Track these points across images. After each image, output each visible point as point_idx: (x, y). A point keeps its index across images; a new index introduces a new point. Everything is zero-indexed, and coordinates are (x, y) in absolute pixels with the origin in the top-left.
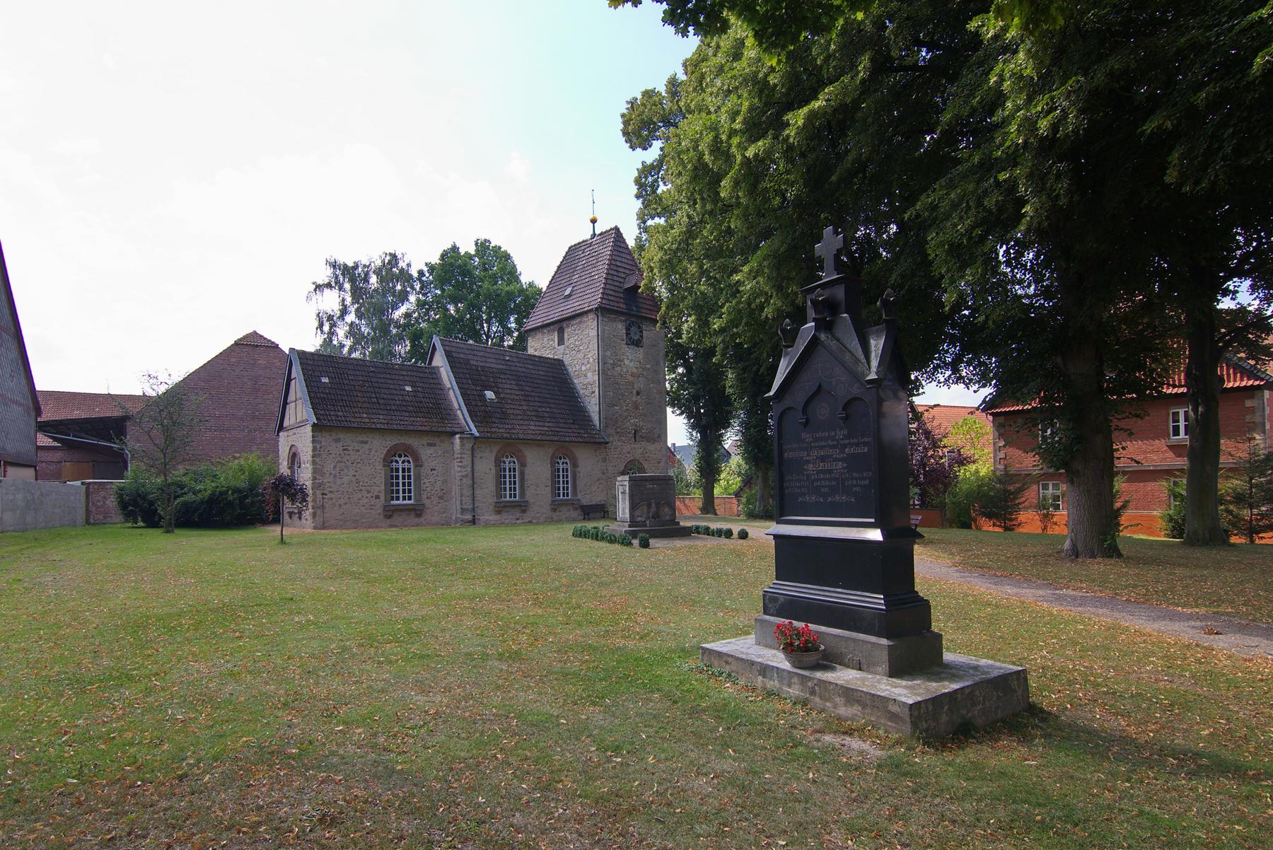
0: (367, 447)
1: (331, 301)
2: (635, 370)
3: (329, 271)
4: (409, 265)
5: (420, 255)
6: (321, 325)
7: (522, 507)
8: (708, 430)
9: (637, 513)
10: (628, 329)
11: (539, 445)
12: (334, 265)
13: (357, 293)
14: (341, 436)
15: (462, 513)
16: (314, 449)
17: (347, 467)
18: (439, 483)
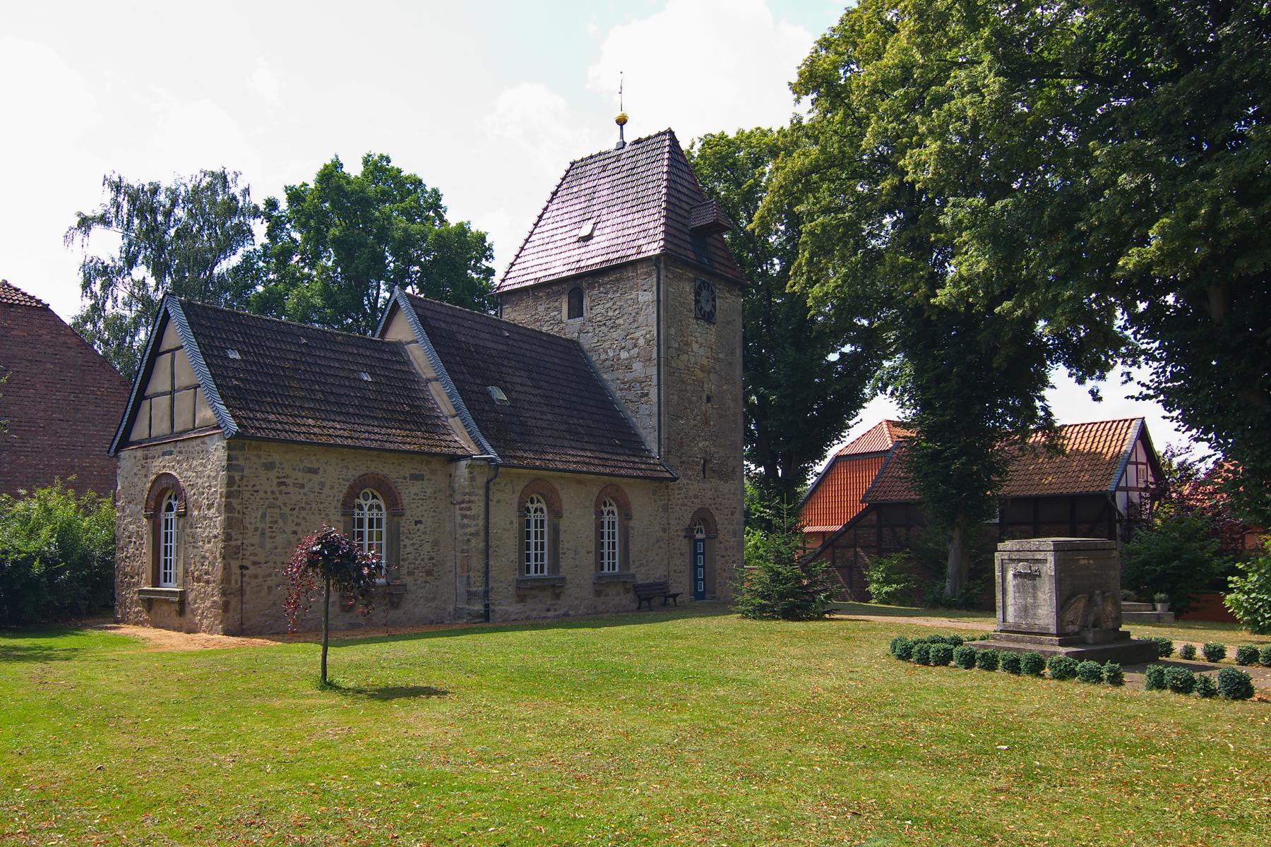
0: (317, 478)
1: (107, 244)
2: (705, 361)
3: (109, 195)
4: (246, 192)
5: (271, 171)
6: (86, 285)
7: (554, 587)
9: (1069, 616)
10: (697, 294)
11: (579, 482)
12: (117, 187)
13: (152, 234)
14: (276, 458)
15: (469, 601)
16: (230, 482)
18: (427, 547)
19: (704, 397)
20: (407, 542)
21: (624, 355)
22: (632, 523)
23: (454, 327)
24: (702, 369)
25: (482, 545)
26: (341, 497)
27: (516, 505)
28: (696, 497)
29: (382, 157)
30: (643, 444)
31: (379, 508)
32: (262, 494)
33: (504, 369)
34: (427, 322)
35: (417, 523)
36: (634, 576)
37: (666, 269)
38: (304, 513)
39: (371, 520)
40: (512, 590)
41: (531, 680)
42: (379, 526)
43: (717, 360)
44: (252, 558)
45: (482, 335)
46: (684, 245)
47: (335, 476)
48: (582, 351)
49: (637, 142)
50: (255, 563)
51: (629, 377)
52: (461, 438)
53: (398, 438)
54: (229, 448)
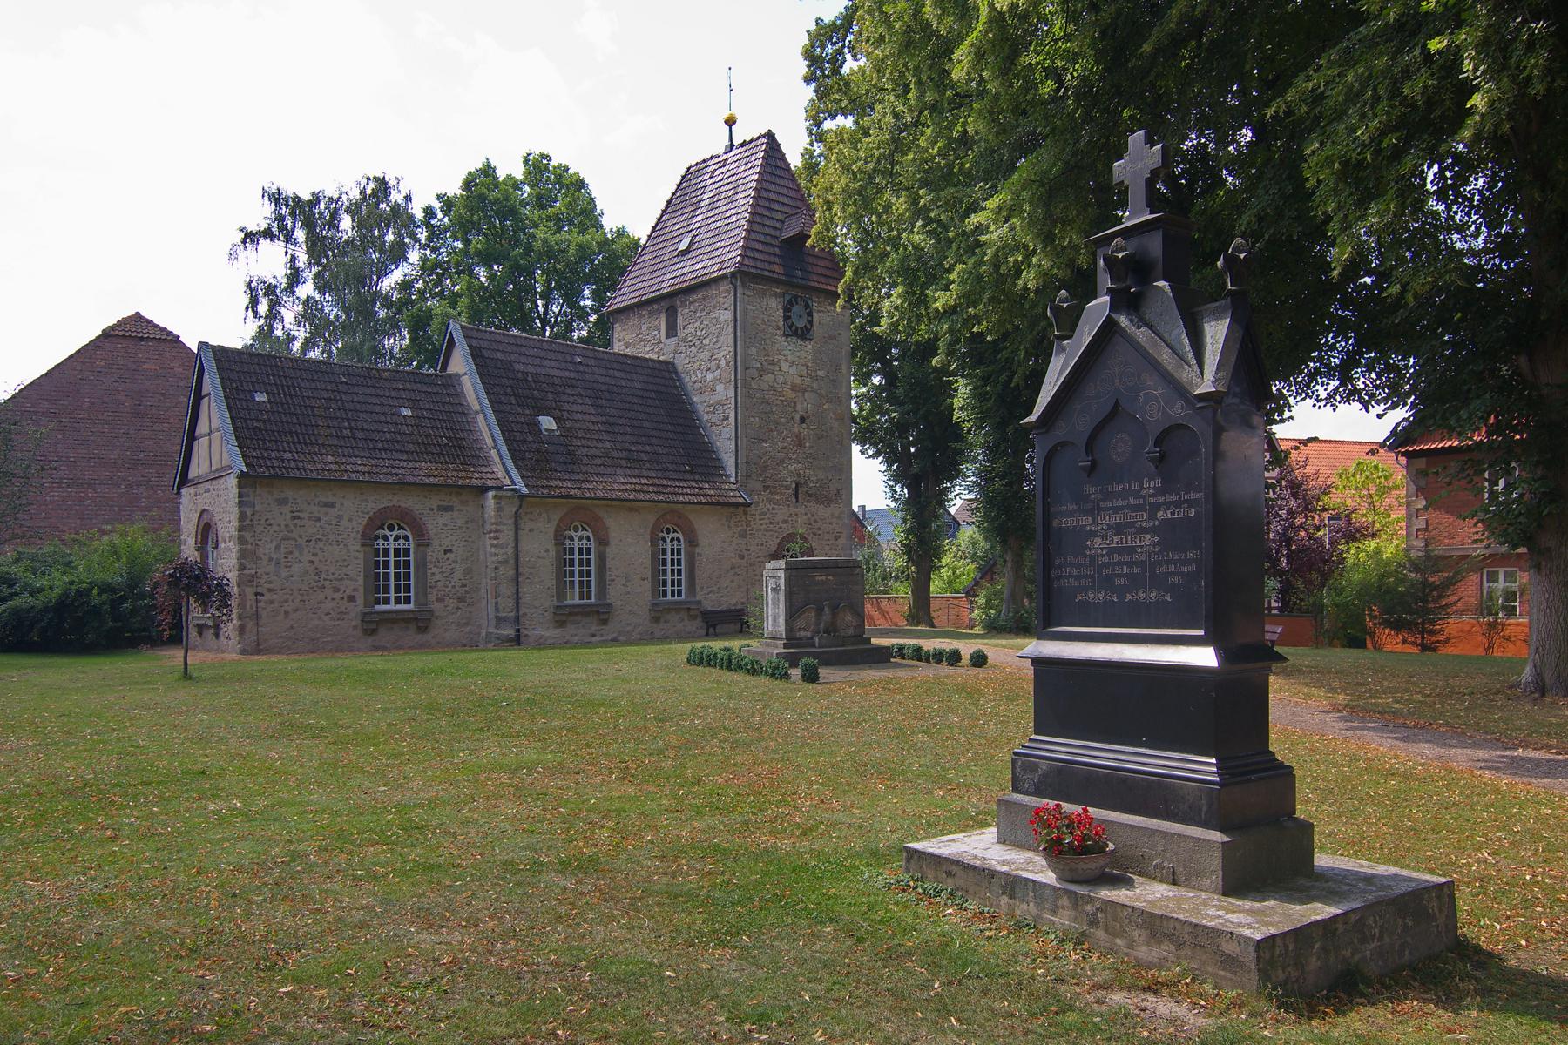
0: (333, 512)
1: (271, 261)
2: (798, 381)
3: (268, 209)
5: (429, 181)
6: (254, 302)
7: (600, 613)
8: (921, 482)
9: (800, 623)
10: (787, 309)
11: (631, 510)
12: (277, 198)
14: (289, 493)
15: (497, 626)
17: (298, 547)
18: (458, 575)
19: (797, 417)
20: (434, 570)
21: (710, 377)
22: (698, 550)
23: (513, 357)
24: (794, 388)
25: (512, 573)
26: (361, 528)
27: (552, 535)
28: (785, 522)
29: (542, 156)
30: (723, 468)
33: (564, 398)
34: (476, 354)
35: (446, 552)
36: (699, 602)
37: (744, 285)
38: (321, 544)
39: (581, 550)
40: (549, 615)
42: (589, 553)
43: (817, 378)
45: (547, 363)
46: (771, 259)
47: (353, 510)
48: (676, 372)
50: (270, 590)
51: (714, 399)
52: (502, 467)
53: (426, 471)
54: (240, 486)
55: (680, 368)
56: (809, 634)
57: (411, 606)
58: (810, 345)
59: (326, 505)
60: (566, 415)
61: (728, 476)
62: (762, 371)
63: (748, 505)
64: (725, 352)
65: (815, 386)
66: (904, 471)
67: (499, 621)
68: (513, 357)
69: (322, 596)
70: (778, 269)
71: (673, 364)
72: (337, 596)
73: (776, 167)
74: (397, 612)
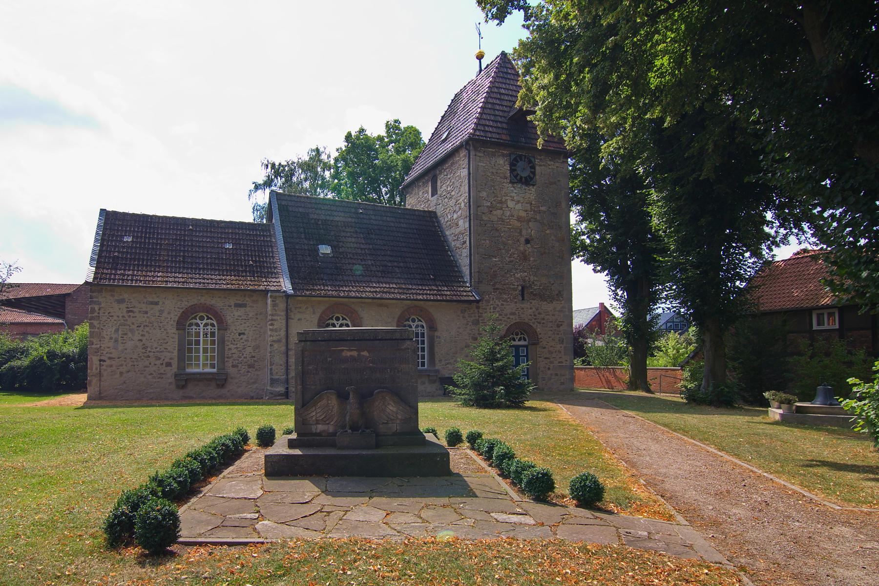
0: (157, 308)
2: (523, 214)
5: (333, 145)
8: (636, 287)
9: (315, 414)
10: (512, 165)
11: (381, 305)
14: (126, 296)
17: (131, 331)
19: (523, 240)
20: (231, 346)
21: (455, 216)
22: (436, 334)
23: (310, 211)
24: (519, 219)
25: (284, 348)
28: (513, 314)
29: (396, 121)
30: (462, 277)
31: (213, 325)
32: (115, 318)
36: (438, 371)
37: (476, 149)
38: (147, 329)
41: (704, 437)
44: (109, 355)
47: (172, 308)
49: (488, 66)
50: (110, 358)
51: (458, 230)
55: (439, 214)
56: (331, 429)
57: (215, 370)
58: (533, 189)
59: (152, 303)
60: (341, 244)
61: (465, 282)
62: (491, 209)
63: (478, 302)
64: (463, 199)
65: (538, 217)
66: (621, 278)
67: (273, 382)
68: (310, 211)
69: (147, 363)
70: (504, 137)
71: (435, 213)
72: (158, 362)
73: (507, 73)
74: (200, 374)
